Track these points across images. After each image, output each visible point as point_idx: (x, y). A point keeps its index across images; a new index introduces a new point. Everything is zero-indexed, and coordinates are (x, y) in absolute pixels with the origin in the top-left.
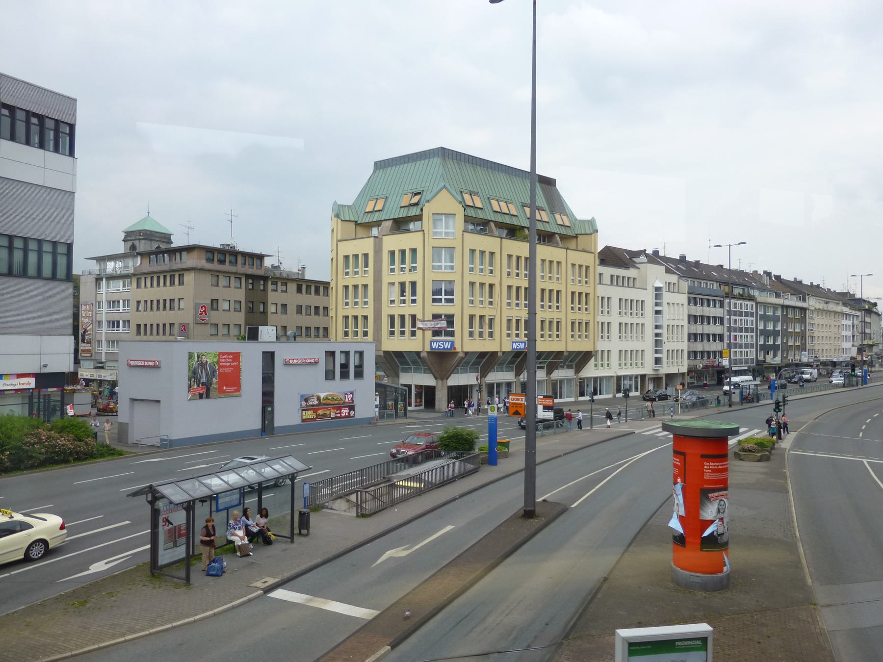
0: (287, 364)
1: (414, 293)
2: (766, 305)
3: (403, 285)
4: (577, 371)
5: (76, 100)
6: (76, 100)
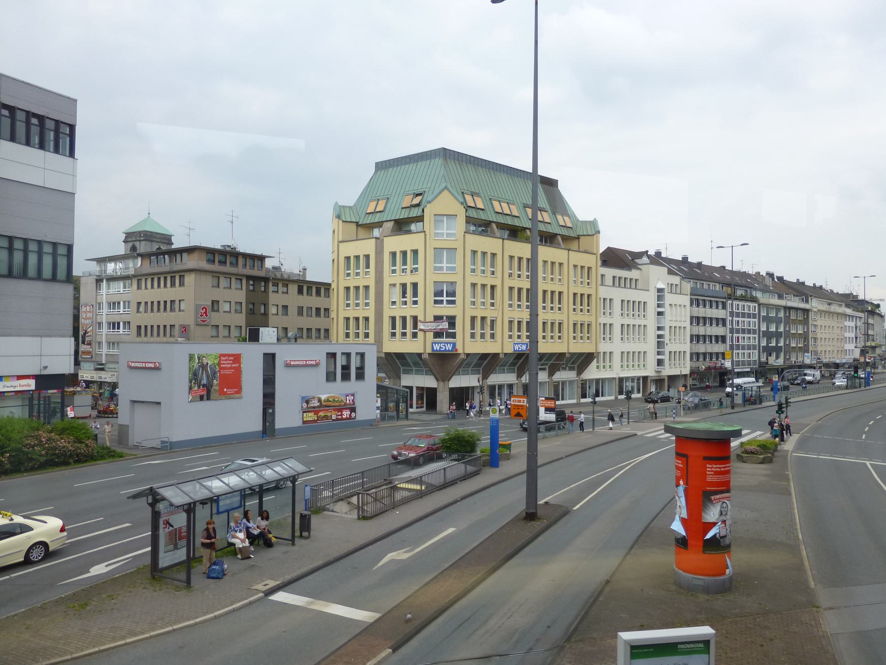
0: (288, 365)
1: (415, 294)
2: (768, 306)
3: (404, 286)
4: (579, 373)
5: (76, 101)
6: (76, 101)
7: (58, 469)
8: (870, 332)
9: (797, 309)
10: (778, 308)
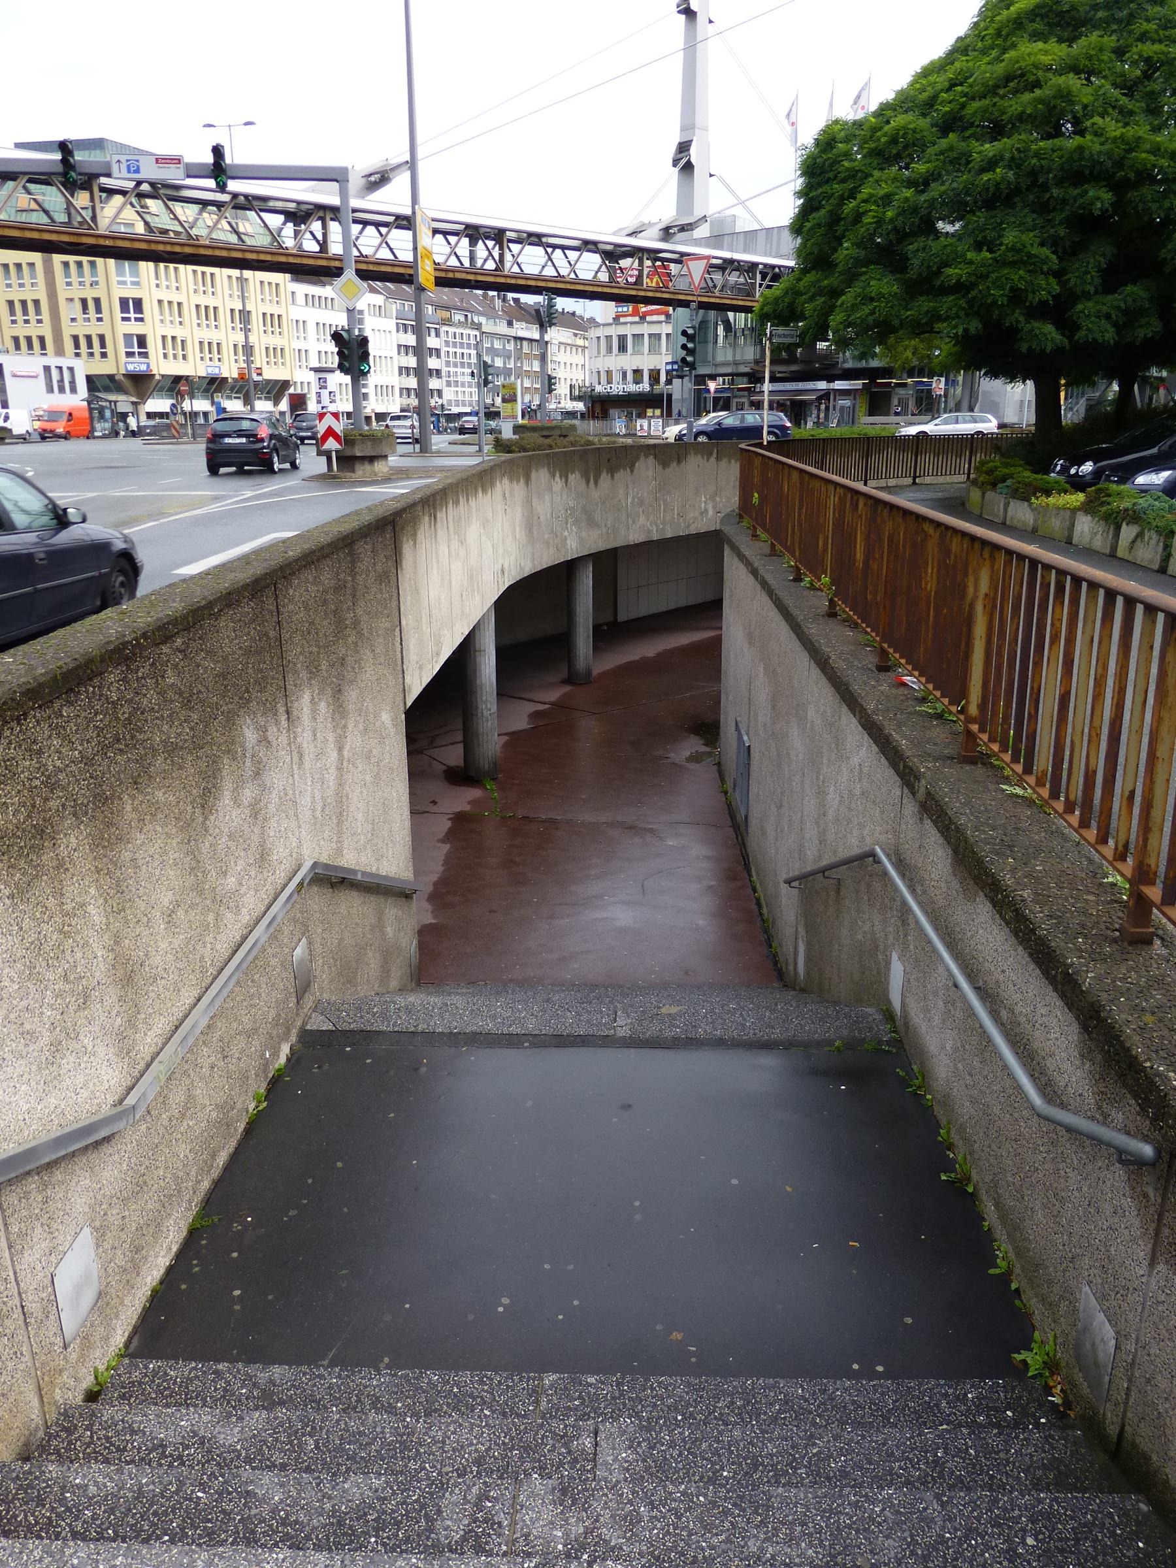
0: (15, 376)
3: (84, 302)
7: (336, 530)
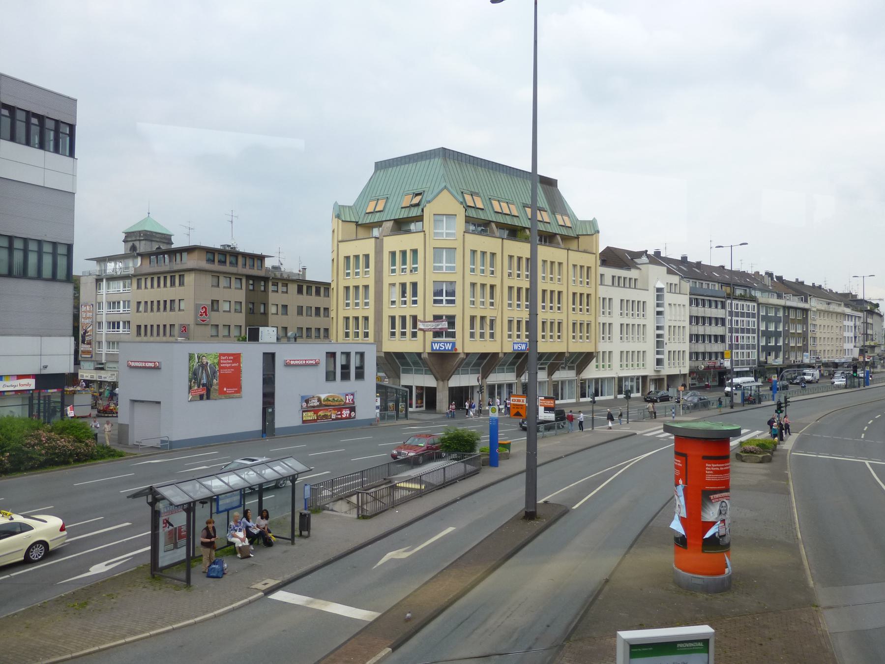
0: (287, 365)
1: (415, 294)
2: (767, 306)
3: (403, 285)
4: (579, 373)
5: (76, 100)
6: (76, 100)
8: (869, 332)
9: (796, 309)
10: (777, 307)
